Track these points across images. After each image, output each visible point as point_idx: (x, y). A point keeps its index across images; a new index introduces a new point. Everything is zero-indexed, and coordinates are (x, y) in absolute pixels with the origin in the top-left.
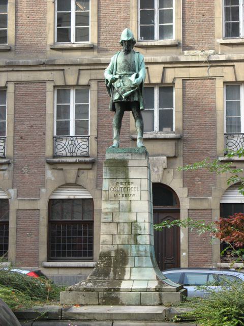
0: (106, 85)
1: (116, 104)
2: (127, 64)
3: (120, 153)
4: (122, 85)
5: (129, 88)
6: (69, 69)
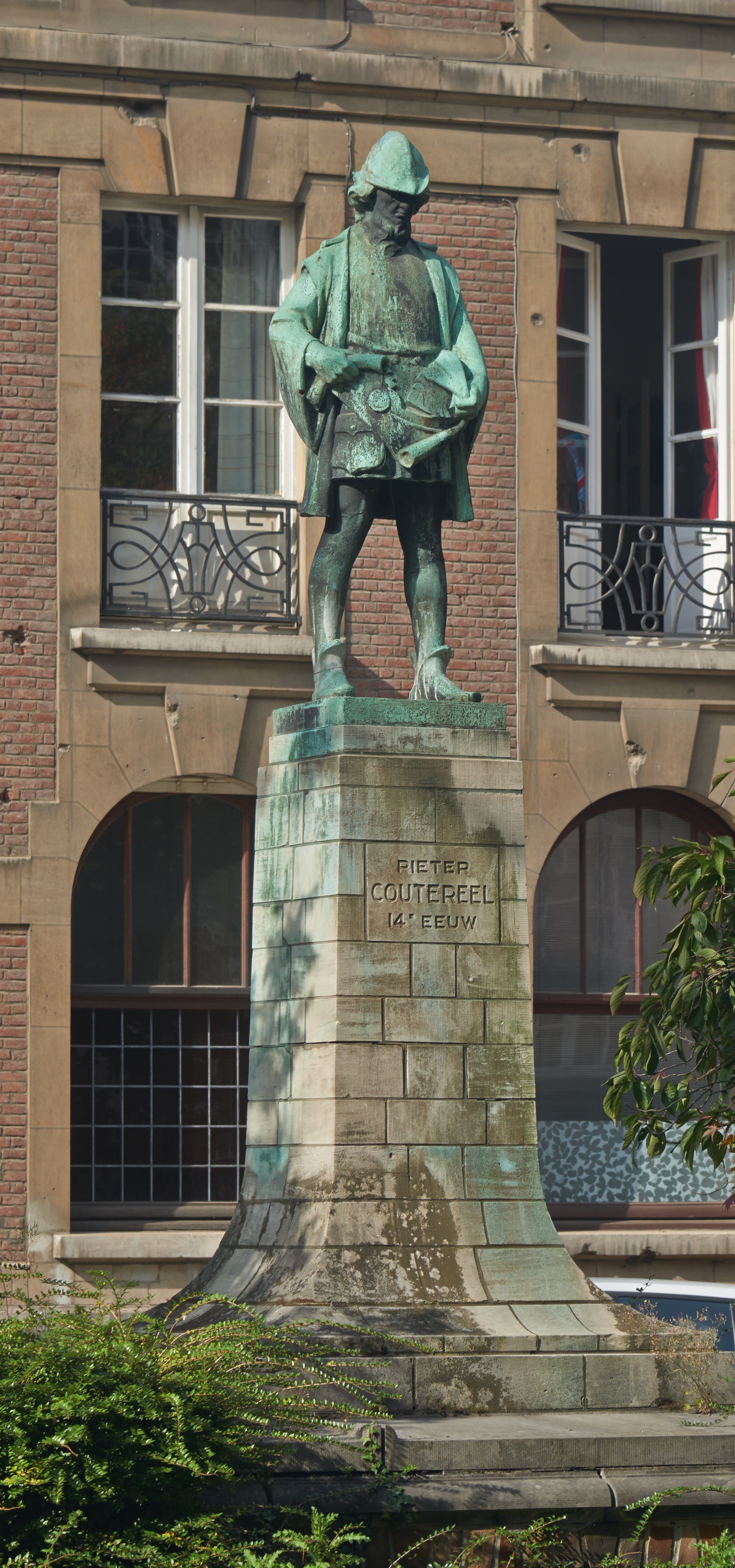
0: (304, 391)
1: (344, 490)
2: (408, 304)
3: (403, 723)
4: (397, 403)
5: (429, 422)
6: (577, 149)
